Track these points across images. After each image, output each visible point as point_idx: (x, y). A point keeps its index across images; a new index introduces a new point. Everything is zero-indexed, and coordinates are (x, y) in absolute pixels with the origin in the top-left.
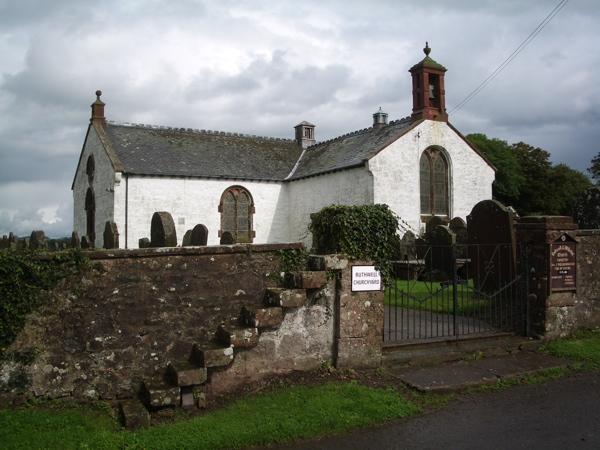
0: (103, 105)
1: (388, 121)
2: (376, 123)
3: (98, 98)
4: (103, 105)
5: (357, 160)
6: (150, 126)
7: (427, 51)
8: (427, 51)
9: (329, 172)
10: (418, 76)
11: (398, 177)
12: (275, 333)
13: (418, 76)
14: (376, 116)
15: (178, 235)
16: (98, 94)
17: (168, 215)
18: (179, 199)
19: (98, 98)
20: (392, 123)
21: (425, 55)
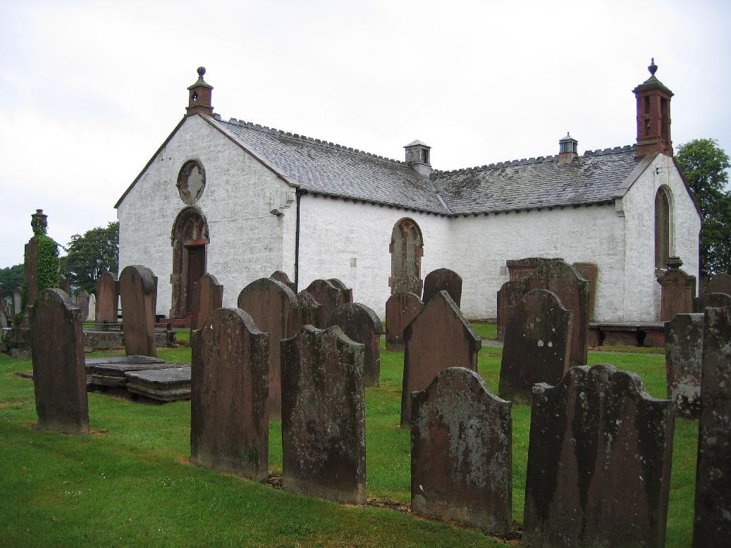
0: (209, 89)
1: (580, 152)
2: (564, 152)
3: (201, 77)
4: (209, 89)
5: (605, 194)
6: (696, 141)
7: (653, 69)
8: (653, 69)
9: (518, 211)
10: (647, 99)
11: (640, 216)
12: (644, 316)
13: (647, 99)
14: (564, 143)
15: (689, 203)
16: (201, 71)
17: (669, 190)
18: (352, 231)
19: (201, 77)
20: (588, 154)
21: (649, 75)
